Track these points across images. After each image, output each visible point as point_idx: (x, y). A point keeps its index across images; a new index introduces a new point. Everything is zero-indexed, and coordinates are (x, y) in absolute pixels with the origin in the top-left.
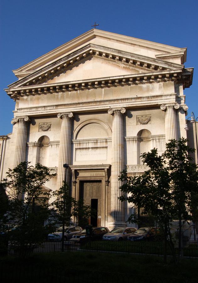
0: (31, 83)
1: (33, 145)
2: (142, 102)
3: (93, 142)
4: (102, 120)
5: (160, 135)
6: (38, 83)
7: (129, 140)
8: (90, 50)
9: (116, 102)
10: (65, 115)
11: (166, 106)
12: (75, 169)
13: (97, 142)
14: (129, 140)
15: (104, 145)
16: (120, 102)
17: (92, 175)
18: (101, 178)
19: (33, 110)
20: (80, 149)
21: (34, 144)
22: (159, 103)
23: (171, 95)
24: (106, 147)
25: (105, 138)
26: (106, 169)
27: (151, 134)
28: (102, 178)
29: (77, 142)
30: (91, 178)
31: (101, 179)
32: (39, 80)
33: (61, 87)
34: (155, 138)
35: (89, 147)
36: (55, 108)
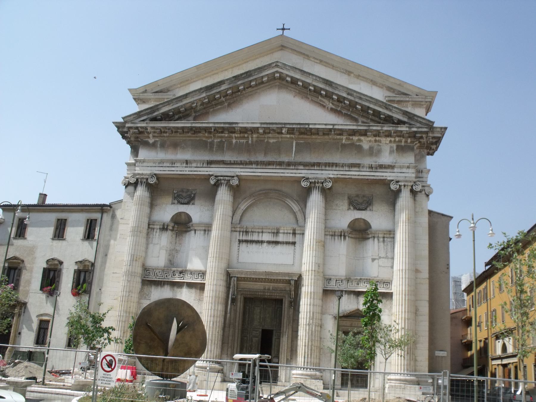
8: (277, 72)
15: (290, 239)
20: (247, 241)
22: (389, 178)
24: (294, 243)
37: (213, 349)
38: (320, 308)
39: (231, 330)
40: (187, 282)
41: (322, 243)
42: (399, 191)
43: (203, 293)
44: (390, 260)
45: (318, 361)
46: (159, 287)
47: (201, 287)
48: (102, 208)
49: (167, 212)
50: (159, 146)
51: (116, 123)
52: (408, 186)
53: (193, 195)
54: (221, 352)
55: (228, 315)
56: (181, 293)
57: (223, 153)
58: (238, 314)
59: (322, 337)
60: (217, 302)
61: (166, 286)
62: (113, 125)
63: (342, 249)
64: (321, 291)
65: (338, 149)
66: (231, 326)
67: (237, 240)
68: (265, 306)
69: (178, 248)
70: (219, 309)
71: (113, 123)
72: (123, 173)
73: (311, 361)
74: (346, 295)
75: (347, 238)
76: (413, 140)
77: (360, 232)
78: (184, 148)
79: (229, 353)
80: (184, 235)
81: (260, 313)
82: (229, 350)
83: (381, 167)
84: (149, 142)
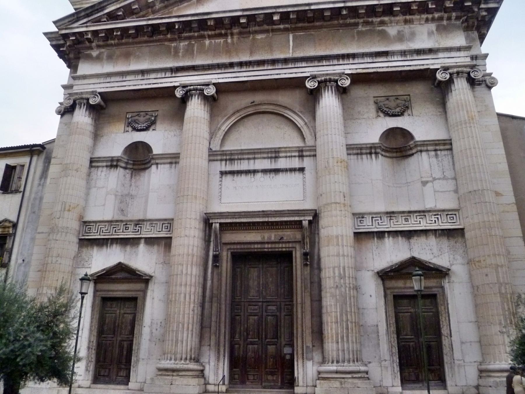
0: (112, 16)
1: (109, 164)
2: (390, 64)
3: (265, 156)
5: (438, 140)
7: (359, 151)
10: (196, 90)
11: (450, 71)
12: (219, 221)
13: (276, 157)
14: (359, 151)
15: (296, 163)
16: (335, 62)
17: (266, 238)
18: (291, 245)
19: (113, 79)
20: (232, 173)
22: (432, 67)
23: (459, 49)
26: (307, 222)
27: (412, 137)
28: (294, 245)
30: (263, 246)
31: (290, 249)
33: (187, 26)
34: (425, 148)
36: (168, 74)
37: (185, 338)
38: (353, 260)
39: (215, 305)
40: (146, 238)
42: (450, 81)
44: (450, 181)
46: (105, 248)
47: (166, 243)
49: (117, 140)
50: (105, 57)
52: (462, 72)
53: (153, 118)
54: (200, 342)
55: (209, 283)
56: (137, 255)
57: (193, 58)
58: (224, 279)
59: (360, 306)
60: (190, 263)
61: (114, 246)
62: (45, 38)
63: (376, 167)
64: (352, 235)
65: (353, 37)
66: (215, 299)
67: (218, 172)
68: (265, 266)
69: (133, 193)
70: (194, 273)
71: (45, 34)
72: (59, 97)
73: (348, 348)
74: (391, 238)
75: (380, 156)
76: (459, 14)
77: (139, 158)
79: (213, 343)
80: (142, 174)
81: (259, 277)
82: (213, 337)
83: (419, 52)
84: (92, 56)
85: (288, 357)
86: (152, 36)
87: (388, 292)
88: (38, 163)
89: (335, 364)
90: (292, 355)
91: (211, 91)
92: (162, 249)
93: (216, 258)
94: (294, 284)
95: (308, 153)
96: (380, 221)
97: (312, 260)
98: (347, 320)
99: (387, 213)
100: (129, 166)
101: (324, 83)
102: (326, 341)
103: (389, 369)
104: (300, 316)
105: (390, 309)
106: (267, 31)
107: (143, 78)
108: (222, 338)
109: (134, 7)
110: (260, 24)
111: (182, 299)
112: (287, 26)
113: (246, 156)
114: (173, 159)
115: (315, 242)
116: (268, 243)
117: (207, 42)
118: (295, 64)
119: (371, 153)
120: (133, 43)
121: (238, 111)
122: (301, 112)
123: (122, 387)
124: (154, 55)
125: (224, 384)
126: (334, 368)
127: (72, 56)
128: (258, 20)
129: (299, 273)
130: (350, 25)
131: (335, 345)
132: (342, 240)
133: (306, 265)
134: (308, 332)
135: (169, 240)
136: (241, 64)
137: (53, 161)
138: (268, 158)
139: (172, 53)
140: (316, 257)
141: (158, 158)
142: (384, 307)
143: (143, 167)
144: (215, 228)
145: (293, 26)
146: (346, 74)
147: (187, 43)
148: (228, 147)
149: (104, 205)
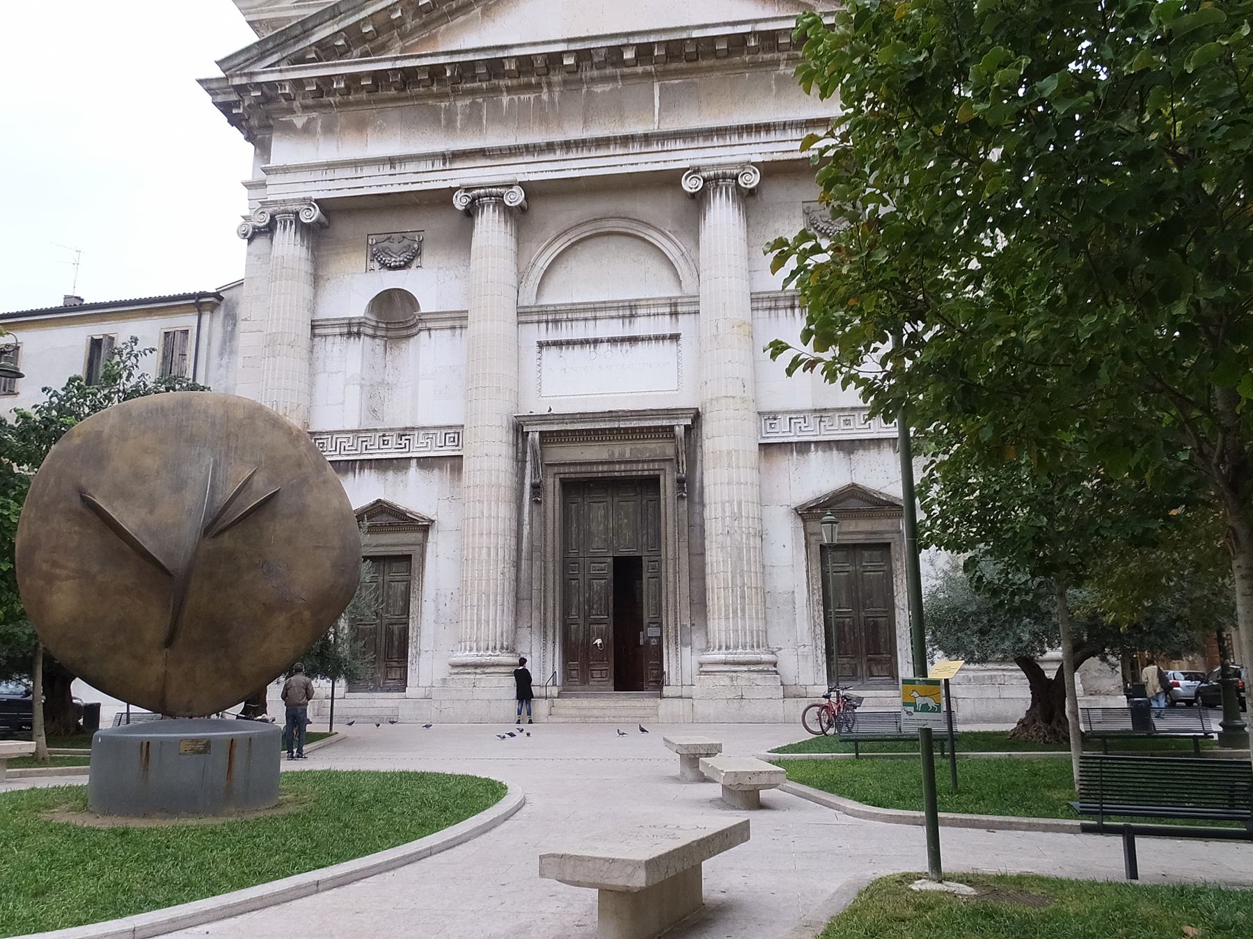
0: (326, 50)
3: (614, 313)
4: (652, 222)
6: (356, 52)
7: (773, 304)
9: (715, 142)
12: (539, 428)
13: (632, 316)
14: (773, 304)
15: (665, 326)
16: (735, 139)
19: (339, 173)
20: (558, 344)
21: (350, 325)
24: (675, 337)
25: (670, 298)
28: (662, 465)
29: (545, 317)
30: (611, 468)
32: (364, 39)
33: (466, 70)
35: (598, 336)
36: (439, 165)
39: (537, 564)
40: (418, 458)
41: (747, 328)
43: (460, 479)
45: (761, 624)
47: (455, 463)
48: (201, 303)
49: (355, 287)
50: (319, 129)
51: (211, 80)
54: (516, 622)
59: (767, 563)
68: (616, 499)
69: (390, 379)
71: (200, 81)
72: (239, 207)
73: (744, 628)
74: (820, 453)
77: (394, 318)
78: (382, 129)
79: (535, 623)
80: (403, 346)
81: (606, 517)
85: (654, 642)
86: (403, 90)
87: (813, 539)
88: (213, 324)
89: (723, 650)
90: (660, 638)
91: (516, 198)
92: (447, 475)
93: (536, 488)
94: (663, 529)
95: (685, 309)
96: (803, 425)
97: (688, 487)
98: (744, 584)
99: (815, 410)
100: (379, 333)
101: (712, 183)
102: (710, 615)
103: (810, 659)
104: (671, 578)
105: (814, 567)
106: (613, 78)
107: (393, 171)
108: (550, 615)
109: (365, 30)
110: (600, 66)
111: (484, 556)
112: (648, 68)
113: (582, 315)
114: (457, 320)
115: (695, 462)
116: (620, 463)
117: (505, 99)
118: (663, 145)
119: (793, 307)
120: (368, 102)
121: (565, 232)
122: (675, 233)
123: (396, 695)
124: (410, 125)
125: (554, 685)
126: (721, 656)
127: (254, 122)
128: (596, 60)
129: (670, 510)
130: (765, 64)
131: (723, 622)
132: (738, 458)
133: (682, 497)
134: (685, 602)
135: (457, 461)
136: (567, 145)
137: (242, 326)
138: (619, 317)
139: (443, 122)
140: (698, 485)
141: (430, 320)
142: (805, 563)
143: (405, 333)
144: (533, 440)
145: (660, 69)
146: (753, 164)
147: (468, 102)
148: (552, 298)
149: (343, 403)
